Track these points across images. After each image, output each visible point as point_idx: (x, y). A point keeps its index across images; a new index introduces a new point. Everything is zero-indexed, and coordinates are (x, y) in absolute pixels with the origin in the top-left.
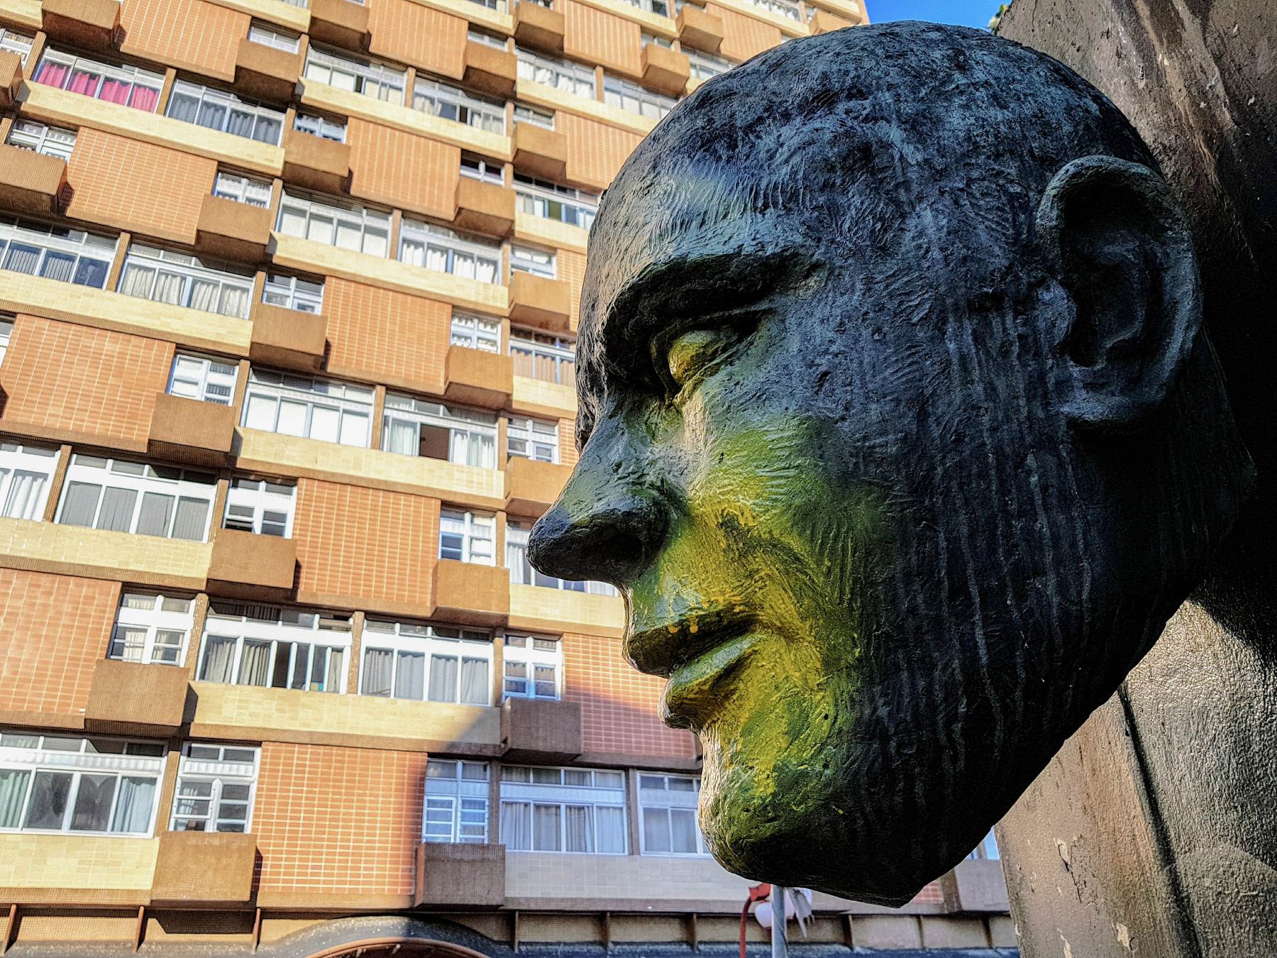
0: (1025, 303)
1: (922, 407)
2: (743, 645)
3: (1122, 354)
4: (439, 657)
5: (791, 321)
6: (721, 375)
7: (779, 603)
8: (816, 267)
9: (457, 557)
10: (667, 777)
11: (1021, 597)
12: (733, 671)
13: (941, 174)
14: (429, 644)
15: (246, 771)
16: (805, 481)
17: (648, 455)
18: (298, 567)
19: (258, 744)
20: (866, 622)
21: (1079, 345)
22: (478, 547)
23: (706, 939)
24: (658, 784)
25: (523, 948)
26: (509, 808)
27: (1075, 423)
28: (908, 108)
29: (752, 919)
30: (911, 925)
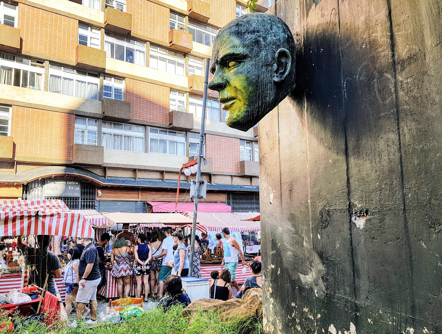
0: (272, 65)
1: (259, 77)
2: (235, 101)
3: (281, 73)
4: (79, 81)
5: (246, 63)
6: (236, 68)
7: (240, 97)
8: (250, 57)
9: (86, 44)
10: (159, 129)
11: (265, 99)
12: (233, 104)
13: (266, 47)
14: (75, 76)
16: (245, 84)
17: (224, 75)
18: (21, 40)
19: (11, 106)
20: (249, 100)
21: (277, 72)
22: (93, 41)
24: (156, 132)
25: (109, 178)
26: (104, 135)
27: (274, 81)
28: (264, 36)
29: (183, 174)
30: (229, 178)
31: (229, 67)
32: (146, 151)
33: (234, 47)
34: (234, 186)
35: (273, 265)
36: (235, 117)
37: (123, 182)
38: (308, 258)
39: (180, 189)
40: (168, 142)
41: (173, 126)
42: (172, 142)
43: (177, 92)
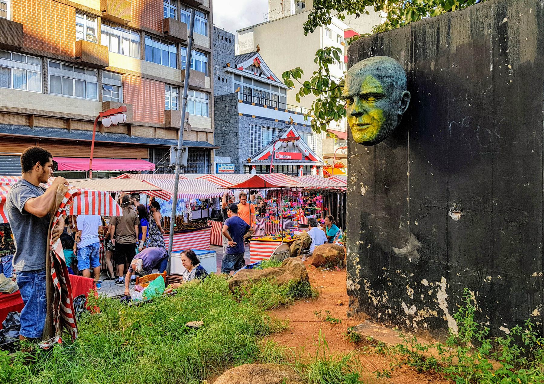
15: (22, 66)
16: (381, 116)
23: (74, 128)
24: (58, 66)
30: (152, 130)
31: (368, 100)
32: (45, 91)
33: (377, 87)
34: (158, 140)
35: (361, 241)
36: (368, 138)
37: (16, 131)
38: (404, 237)
39: (95, 142)
40: (74, 81)
41: (85, 63)
42: (80, 82)
43: (85, 16)
